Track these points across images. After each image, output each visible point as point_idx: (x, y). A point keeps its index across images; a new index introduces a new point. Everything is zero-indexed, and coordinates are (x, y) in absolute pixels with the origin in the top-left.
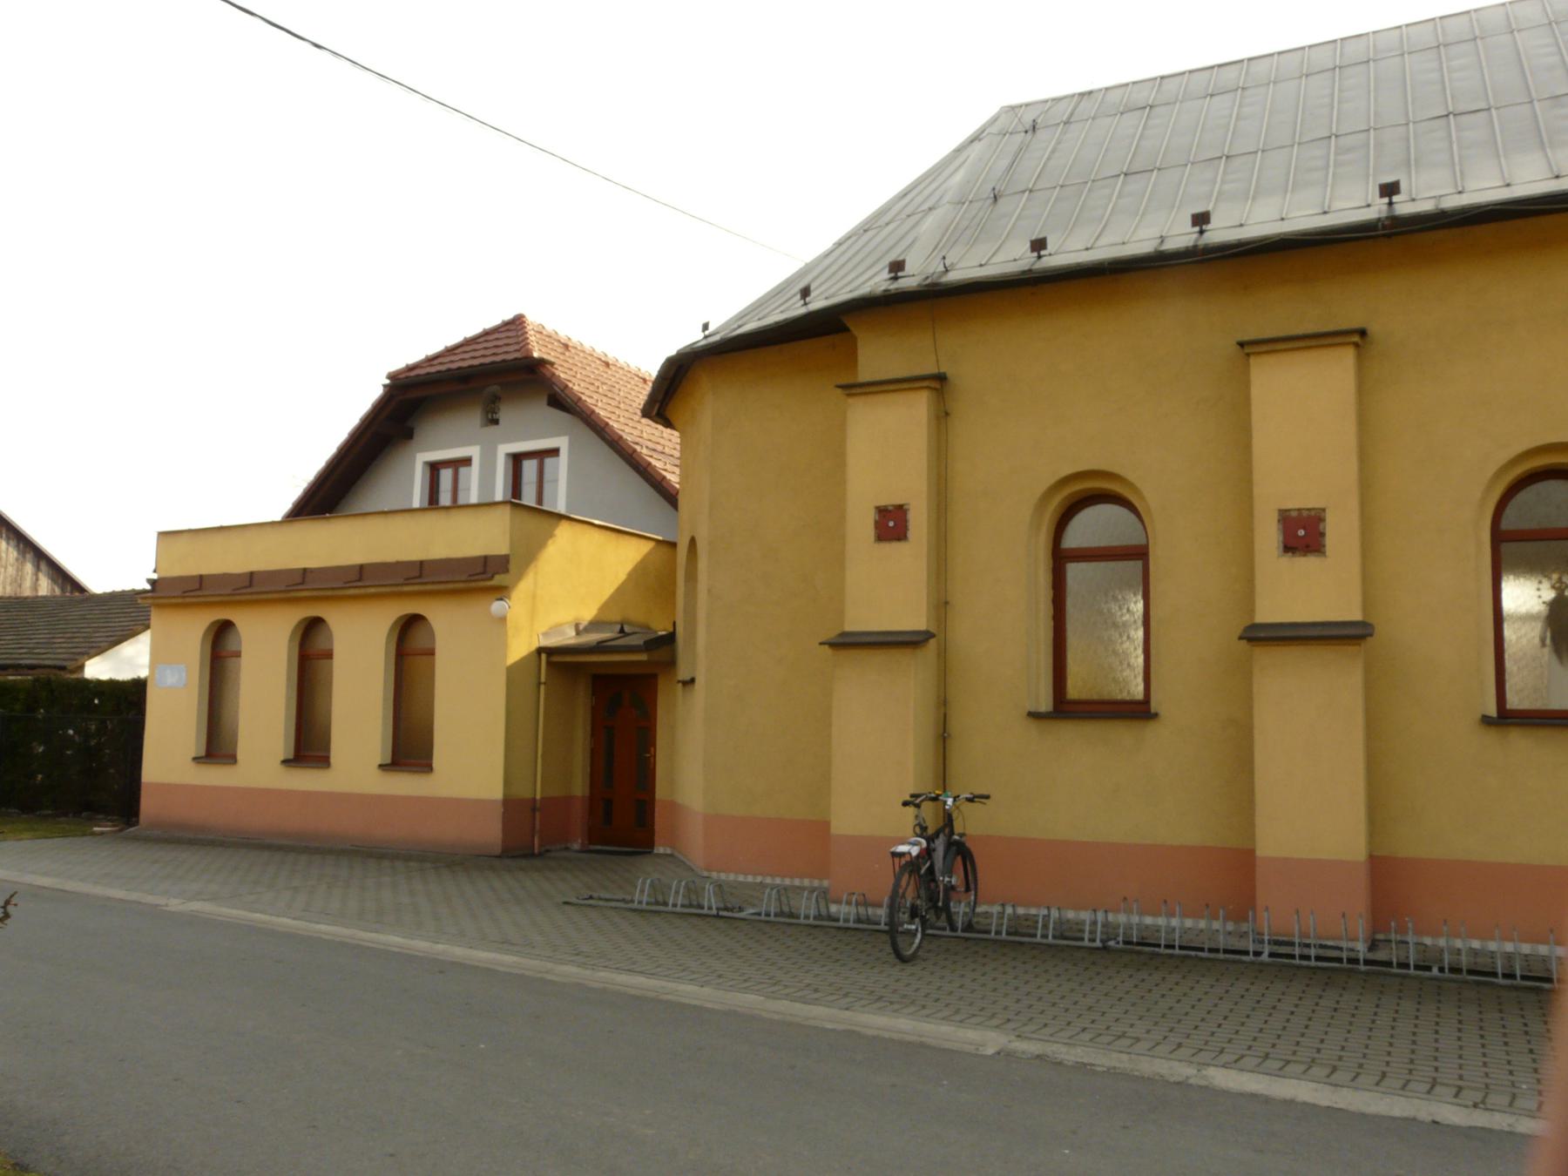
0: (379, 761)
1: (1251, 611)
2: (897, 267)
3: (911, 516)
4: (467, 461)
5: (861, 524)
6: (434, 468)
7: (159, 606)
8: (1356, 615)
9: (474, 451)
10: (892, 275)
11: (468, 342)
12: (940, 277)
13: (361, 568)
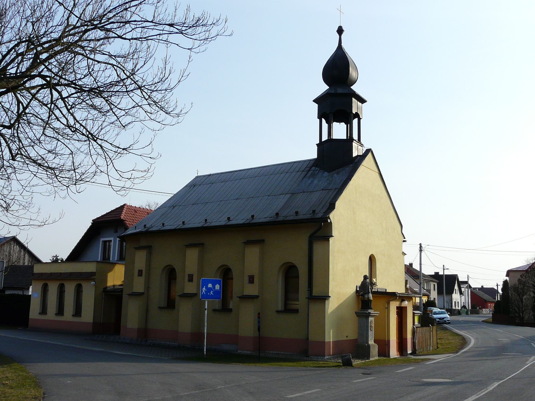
1: (184, 291)
2: (297, 213)
3: (194, 277)
4: (111, 241)
5: (136, 273)
6: (105, 242)
7: (34, 280)
8: (196, 293)
10: (296, 215)
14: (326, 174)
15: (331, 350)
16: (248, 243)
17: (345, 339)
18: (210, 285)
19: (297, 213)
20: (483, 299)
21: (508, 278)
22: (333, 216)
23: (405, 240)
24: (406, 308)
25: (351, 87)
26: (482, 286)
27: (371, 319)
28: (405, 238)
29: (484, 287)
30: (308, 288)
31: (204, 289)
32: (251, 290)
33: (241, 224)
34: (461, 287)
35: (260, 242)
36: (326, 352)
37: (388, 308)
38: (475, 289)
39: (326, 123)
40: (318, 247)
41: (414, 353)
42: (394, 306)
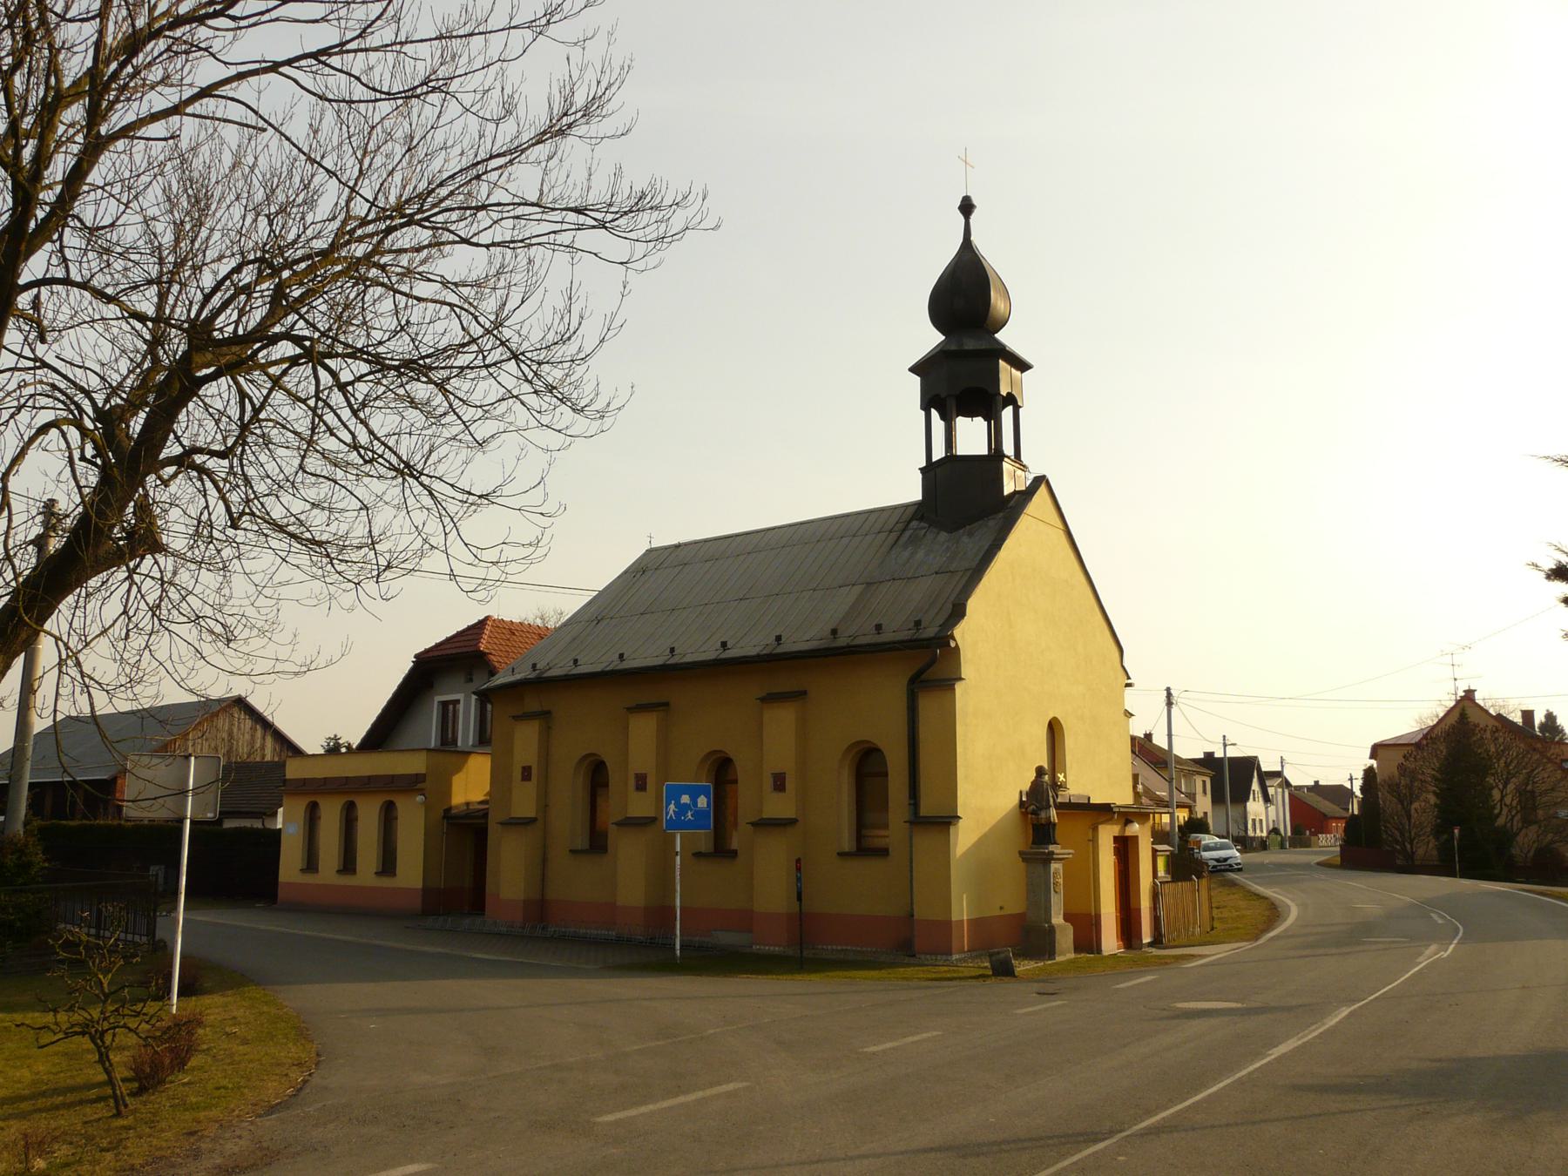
0: (336, 869)
5: (517, 774)
6: (445, 704)
8: (652, 814)
9: (460, 696)
11: (448, 640)
12: (544, 673)
13: (369, 778)
14: (943, 535)
16: (771, 699)
17: (997, 913)
19: (878, 627)
21: (1374, 763)
22: (963, 634)
23: (1129, 681)
26: (1317, 782)
27: (1055, 866)
28: (1129, 678)
29: (1321, 783)
30: (910, 798)
31: (672, 807)
32: (779, 806)
36: (955, 944)
37: (1094, 841)
39: (922, 408)
40: (928, 705)
41: (1157, 941)
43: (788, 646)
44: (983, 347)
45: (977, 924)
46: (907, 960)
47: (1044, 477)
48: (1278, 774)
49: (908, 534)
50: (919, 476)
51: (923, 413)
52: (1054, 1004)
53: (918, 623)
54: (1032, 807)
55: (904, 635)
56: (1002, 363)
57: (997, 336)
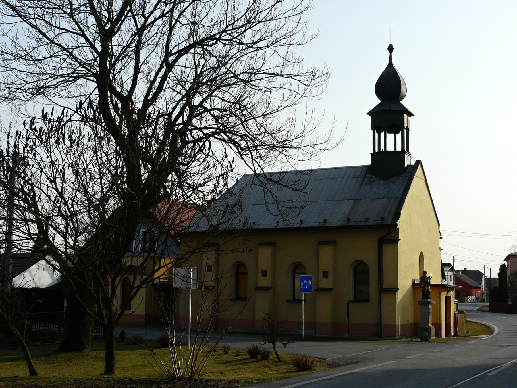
8: (332, 287)
14: (382, 182)
15: (399, 331)
16: (321, 243)
17: (407, 323)
18: (306, 281)
19: (367, 219)
20: (468, 284)
21: (506, 263)
22: (400, 223)
23: (441, 236)
24: (450, 297)
25: (401, 102)
26: (465, 269)
27: (430, 306)
28: (441, 235)
29: (467, 269)
30: (379, 282)
31: (302, 284)
32: (265, 282)
33: (316, 227)
34: (445, 270)
35: (332, 243)
36: (397, 334)
37: (440, 298)
38: (458, 271)
39: (372, 129)
40: (387, 249)
41: (456, 334)
42: (444, 295)
43: (328, 224)
44: (399, 109)
45: (402, 326)
46: (380, 338)
47: (420, 161)
48: (449, 265)
49: (366, 179)
50: (370, 156)
51: (372, 131)
52: (473, 342)
53: (383, 219)
54: (423, 286)
55: (376, 223)
56: (405, 115)
57: (401, 102)
